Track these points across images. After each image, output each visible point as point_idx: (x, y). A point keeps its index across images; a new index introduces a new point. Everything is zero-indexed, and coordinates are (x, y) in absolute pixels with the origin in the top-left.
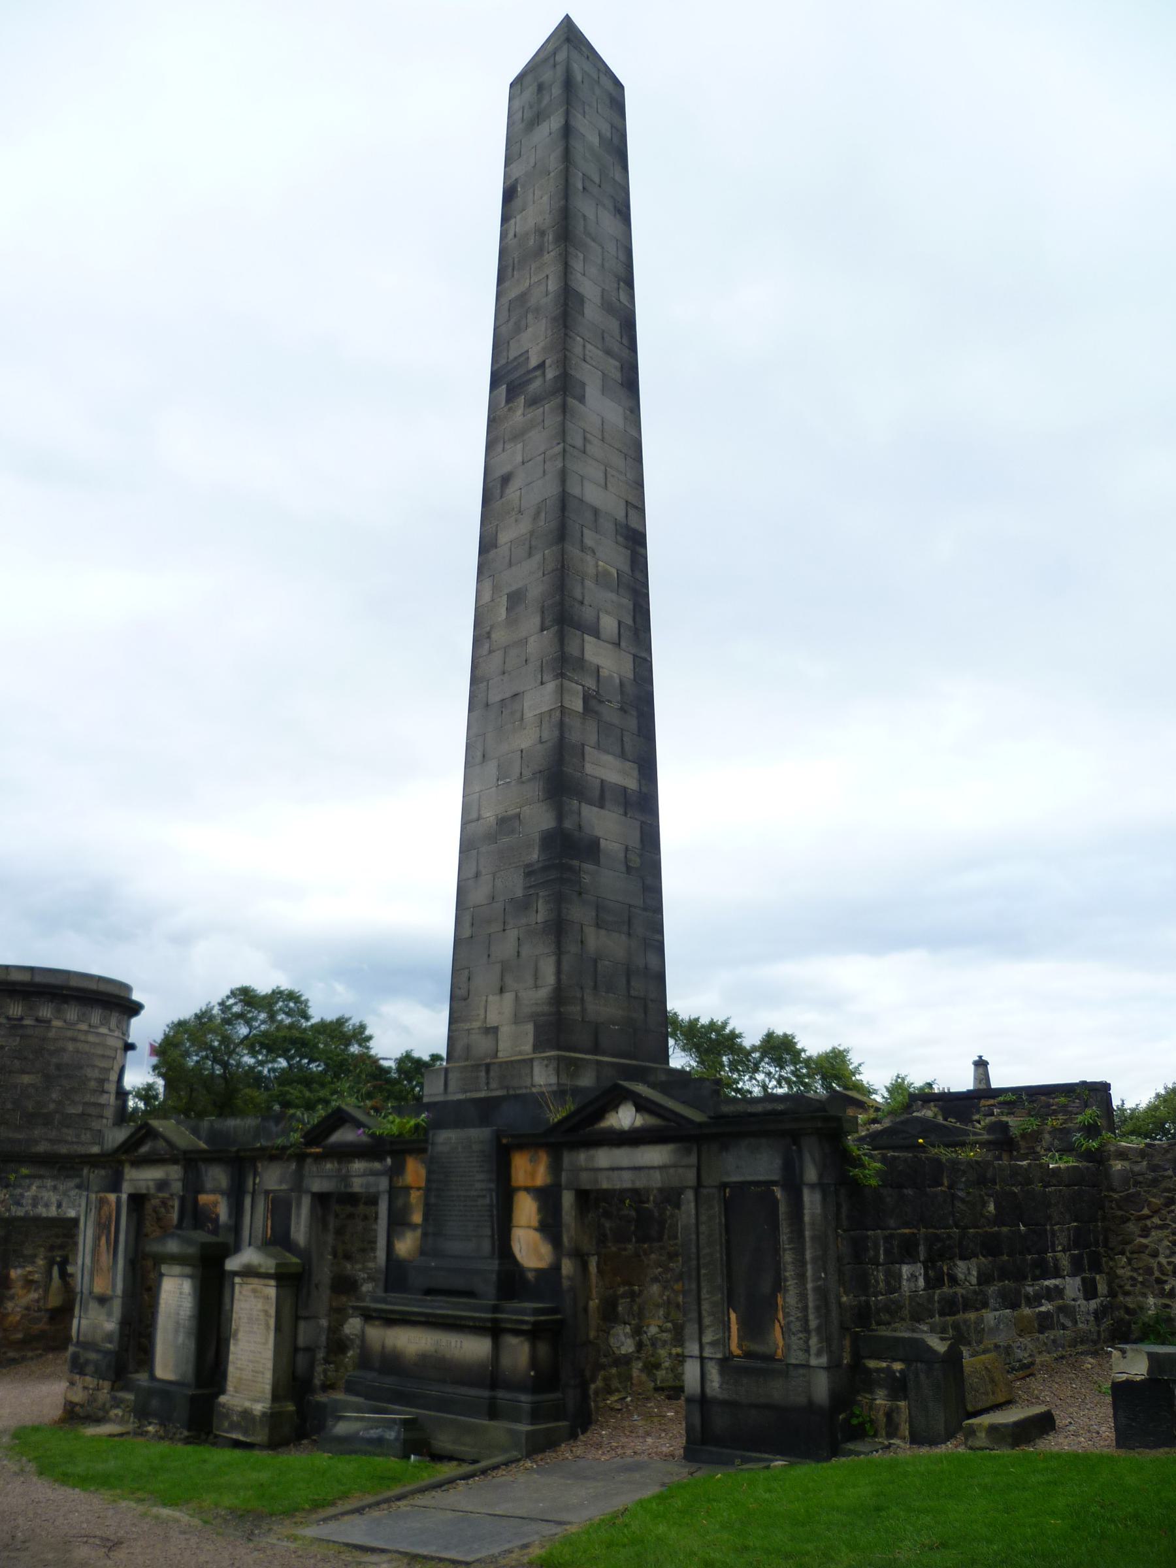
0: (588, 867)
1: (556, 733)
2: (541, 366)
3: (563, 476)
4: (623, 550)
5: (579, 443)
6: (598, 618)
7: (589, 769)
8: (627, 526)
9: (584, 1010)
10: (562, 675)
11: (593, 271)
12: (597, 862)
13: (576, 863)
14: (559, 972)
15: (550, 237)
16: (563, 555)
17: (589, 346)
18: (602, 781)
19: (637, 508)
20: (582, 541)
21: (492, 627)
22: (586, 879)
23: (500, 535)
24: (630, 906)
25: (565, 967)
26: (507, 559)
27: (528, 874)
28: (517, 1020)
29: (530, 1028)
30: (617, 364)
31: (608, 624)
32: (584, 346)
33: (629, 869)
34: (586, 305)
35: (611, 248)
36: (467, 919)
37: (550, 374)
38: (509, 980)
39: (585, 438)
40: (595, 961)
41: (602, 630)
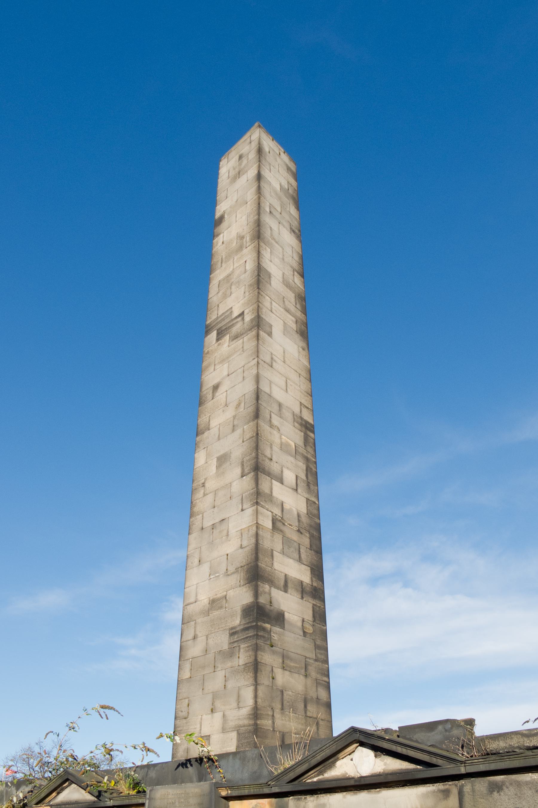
0: (276, 629)
1: (253, 541)
3: (258, 379)
4: (299, 432)
5: (268, 359)
6: (282, 472)
7: (276, 566)
8: (301, 418)
10: (257, 503)
11: (277, 261)
12: (283, 627)
13: (268, 626)
14: (256, 697)
15: (248, 238)
16: (257, 427)
17: (274, 303)
18: (286, 575)
20: (270, 421)
21: (206, 479)
22: (275, 637)
23: (211, 422)
24: (306, 657)
25: (260, 693)
26: (217, 436)
27: (232, 634)
28: (224, 730)
29: (234, 735)
30: (293, 319)
31: (289, 476)
32: (271, 303)
34: (273, 279)
37: (248, 318)
38: (218, 704)
39: (272, 358)
40: (282, 692)
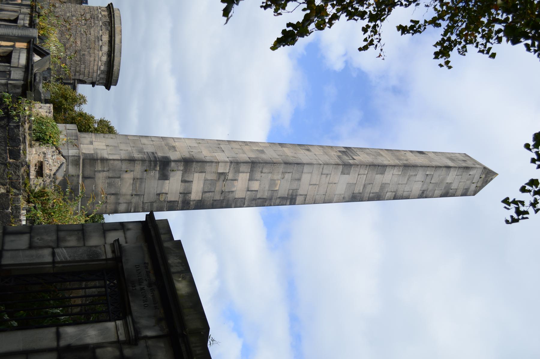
0: (157, 175)
2: (354, 159)
4: (287, 193)
5: (325, 171)
6: (257, 180)
7: (196, 175)
8: (296, 195)
9: (100, 171)
11: (395, 179)
12: (160, 179)
13: (158, 168)
15: (405, 162)
17: (365, 176)
18: (192, 182)
19: (305, 200)
22: (152, 173)
24: (144, 195)
25: (116, 162)
27: (153, 153)
29: (92, 152)
30: (361, 191)
31: (255, 185)
33: (159, 195)
34: (381, 175)
35: (407, 188)
36: (136, 138)
38: (109, 148)
40: (119, 177)
41: (253, 182)
